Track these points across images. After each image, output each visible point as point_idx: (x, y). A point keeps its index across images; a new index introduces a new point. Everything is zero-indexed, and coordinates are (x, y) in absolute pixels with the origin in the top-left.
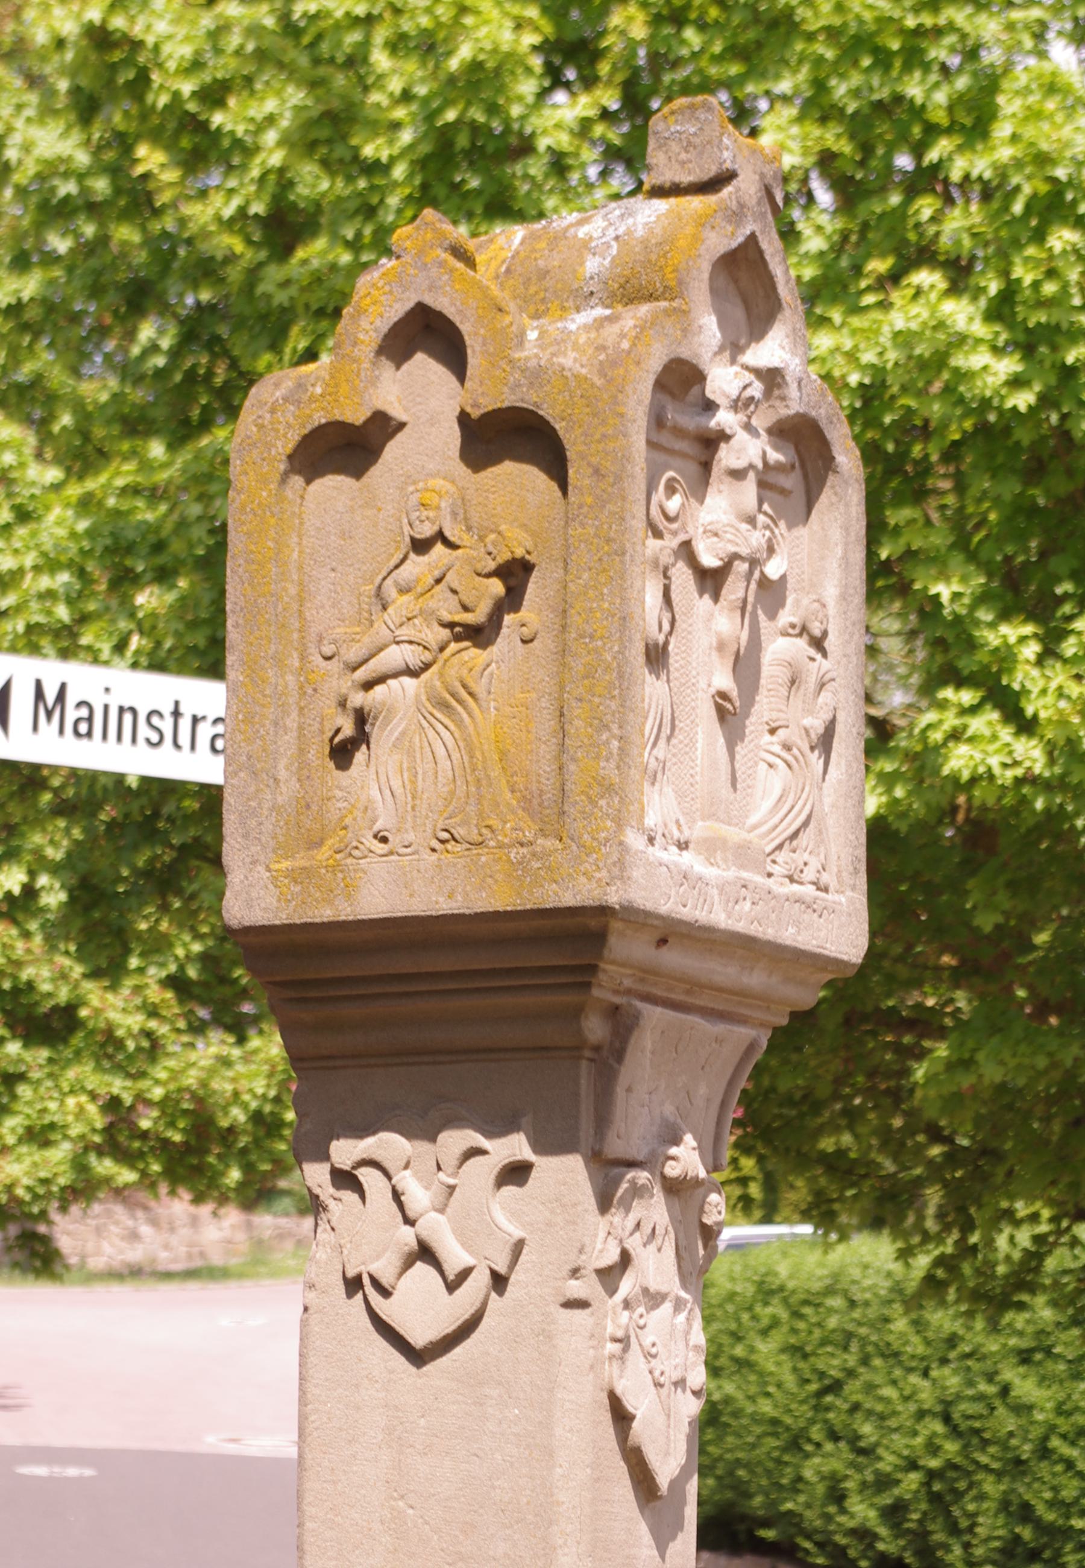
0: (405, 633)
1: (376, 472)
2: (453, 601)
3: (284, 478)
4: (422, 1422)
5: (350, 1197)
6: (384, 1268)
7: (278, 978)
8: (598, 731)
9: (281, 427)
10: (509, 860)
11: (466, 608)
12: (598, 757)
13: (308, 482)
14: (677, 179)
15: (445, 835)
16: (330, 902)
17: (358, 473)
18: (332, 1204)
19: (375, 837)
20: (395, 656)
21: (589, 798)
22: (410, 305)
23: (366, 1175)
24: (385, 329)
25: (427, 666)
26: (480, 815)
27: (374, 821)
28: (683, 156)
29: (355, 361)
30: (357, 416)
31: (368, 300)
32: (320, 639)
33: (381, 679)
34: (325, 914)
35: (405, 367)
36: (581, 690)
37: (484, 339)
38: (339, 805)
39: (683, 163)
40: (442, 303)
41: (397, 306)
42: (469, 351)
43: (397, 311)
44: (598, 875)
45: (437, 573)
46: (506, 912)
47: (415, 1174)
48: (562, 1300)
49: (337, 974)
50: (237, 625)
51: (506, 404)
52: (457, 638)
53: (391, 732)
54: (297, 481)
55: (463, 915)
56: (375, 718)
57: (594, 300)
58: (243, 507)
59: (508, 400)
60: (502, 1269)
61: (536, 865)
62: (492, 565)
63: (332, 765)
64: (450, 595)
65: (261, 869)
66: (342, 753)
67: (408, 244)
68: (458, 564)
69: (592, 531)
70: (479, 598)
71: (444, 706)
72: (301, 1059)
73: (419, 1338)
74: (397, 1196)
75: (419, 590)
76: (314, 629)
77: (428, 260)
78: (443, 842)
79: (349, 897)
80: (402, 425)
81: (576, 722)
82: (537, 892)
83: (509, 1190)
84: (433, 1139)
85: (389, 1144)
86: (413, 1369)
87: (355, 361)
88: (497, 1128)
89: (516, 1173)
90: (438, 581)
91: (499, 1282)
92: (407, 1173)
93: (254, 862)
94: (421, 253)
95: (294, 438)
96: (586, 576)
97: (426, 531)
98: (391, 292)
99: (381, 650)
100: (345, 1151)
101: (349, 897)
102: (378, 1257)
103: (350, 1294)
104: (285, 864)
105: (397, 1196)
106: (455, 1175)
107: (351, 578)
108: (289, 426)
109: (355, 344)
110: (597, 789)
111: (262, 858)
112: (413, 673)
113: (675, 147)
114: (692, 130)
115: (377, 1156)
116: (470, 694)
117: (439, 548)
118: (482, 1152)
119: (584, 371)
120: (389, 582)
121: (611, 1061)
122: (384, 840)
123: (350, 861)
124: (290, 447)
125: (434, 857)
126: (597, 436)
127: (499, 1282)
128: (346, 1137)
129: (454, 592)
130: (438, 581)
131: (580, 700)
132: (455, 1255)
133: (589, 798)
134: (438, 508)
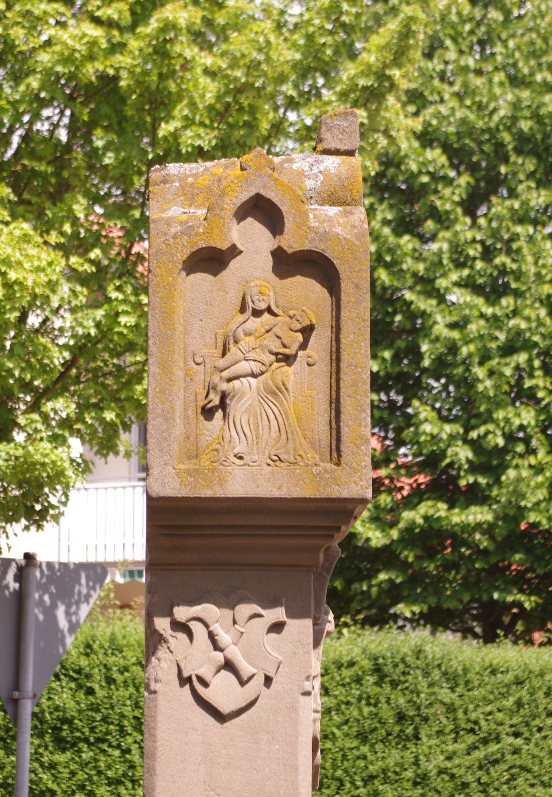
0: (251, 355)
1: (225, 274)
2: (278, 342)
3: (180, 271)
4: (224, 751)
5: (182, 636)
6: (206, 672)
7: (165, 523)
8: (360, 413)
9: (180, 247)
10: (312, 472)
11: (285, 346)
12: (360, 425)
13: (187, 275)
14: (338, 147)
15: (276, 458)
16: (211, 487)
17: (215, 273)
18: (170, 639)
19: (235, 456)
20: (244, 367)
21: (356, 445)
22: (253, 194)
23: (195, 626)
24: (239, 204)
25: (262, 373)
26: (295, 449)
27: (234, 448)
28: (340, 136)
29: (222, 218)
30: (224, 246)
31: (229, 189)
32: (194, 355)
33: (237, 378)
34: (208, 493)
35: (242, 224)
36: (350, 392)
37: (295, 215)
38: (207, 438)
39: (341, 140)
40: (271, 194)
41: (245, 193)
42: (286, 220)
43: (245, 196)
44: (361, 483)
45: (267, 328)
46: (310, 499)
47: (221, 625)
48: (302, 691)
49: (199, 523)
50: (155, 344)
51: (306, 248)
52: (278, 361)
53: (244, 404)
54: (184, 273)
55: (286, 499)
56: (234, 397)
57: (312, 201)
58: (158, 285)
59: (307, 246)
60: (271, 674)
61: (327, 476)
62: (299, 327)
63: (202, 418)
64: (276, 339)
65: (170, 468)
66: (208, 413)
67: (251, 163)
68: (280, 324)
69: (355, 315)
70: (293, 342)
71: (274, 394)
72: (155, 565)
73: (225, 708)
74: (212, 636)
75: (257, 335)
76: (190, 349)
77: (263, 173)
78: (274, 461)
79: (221, 485)
80: (241, 252)
81: (348, 407)
82: (328, 490)
83: (273, 635)
84: (233, 608)
85: (208, 610)
86: (218, 725)
87: (222, 218)
88: (270, 603)
89: (277, 627)
90: (267, 331)
91: (268, 681)
92: (217, 625)
93: (166, 464)
94: (258, 169)
95: (187, 252)
96: (352, 336)
97: (262, 306)
98: (241, 186)
99: (237, 363)
100: (182, 613)
101: (221, 485)
102: (200, 667)
103: (182, 685)
104: (182, 467)
105: (212, 636)
106: (243, 627)
107: (211, 325)
108: (184, 246)
109: (222, 209)
110: (360, 441)
111: (171, 462)
112: (254, 375)
113: (336, 132)
114: (345, 125)
115: (202, 615)
116: (286, 389)
117: (266, 315)
118: (259, 616)
119: (349, 237)
120: (240, 329)
121: (324, 573)
122: (241, 458)
123: (221, 467)
124: (185, 257)
125: (269, 468)
126: (357, 269)
127: (268, 681)
128: (183, 605)
129: (279, 337)
130: (267, 331)
131: (350, 397)
132: (246, 668)
133: (356, 445)
134: (269, 295)
